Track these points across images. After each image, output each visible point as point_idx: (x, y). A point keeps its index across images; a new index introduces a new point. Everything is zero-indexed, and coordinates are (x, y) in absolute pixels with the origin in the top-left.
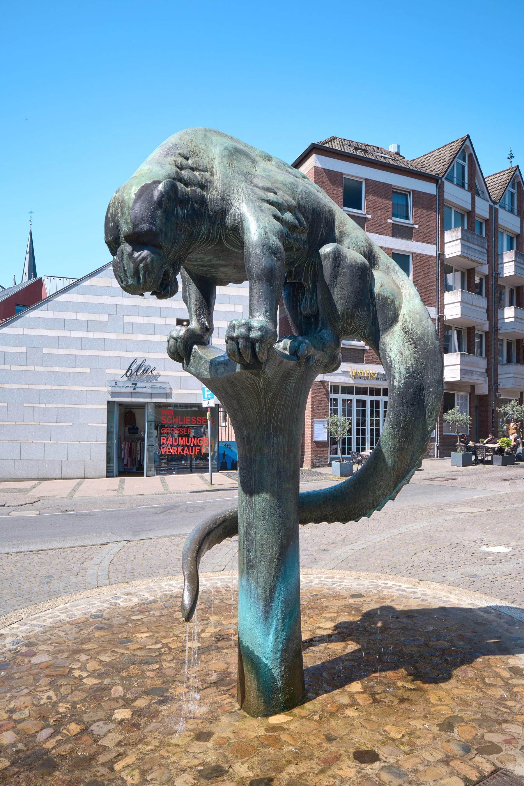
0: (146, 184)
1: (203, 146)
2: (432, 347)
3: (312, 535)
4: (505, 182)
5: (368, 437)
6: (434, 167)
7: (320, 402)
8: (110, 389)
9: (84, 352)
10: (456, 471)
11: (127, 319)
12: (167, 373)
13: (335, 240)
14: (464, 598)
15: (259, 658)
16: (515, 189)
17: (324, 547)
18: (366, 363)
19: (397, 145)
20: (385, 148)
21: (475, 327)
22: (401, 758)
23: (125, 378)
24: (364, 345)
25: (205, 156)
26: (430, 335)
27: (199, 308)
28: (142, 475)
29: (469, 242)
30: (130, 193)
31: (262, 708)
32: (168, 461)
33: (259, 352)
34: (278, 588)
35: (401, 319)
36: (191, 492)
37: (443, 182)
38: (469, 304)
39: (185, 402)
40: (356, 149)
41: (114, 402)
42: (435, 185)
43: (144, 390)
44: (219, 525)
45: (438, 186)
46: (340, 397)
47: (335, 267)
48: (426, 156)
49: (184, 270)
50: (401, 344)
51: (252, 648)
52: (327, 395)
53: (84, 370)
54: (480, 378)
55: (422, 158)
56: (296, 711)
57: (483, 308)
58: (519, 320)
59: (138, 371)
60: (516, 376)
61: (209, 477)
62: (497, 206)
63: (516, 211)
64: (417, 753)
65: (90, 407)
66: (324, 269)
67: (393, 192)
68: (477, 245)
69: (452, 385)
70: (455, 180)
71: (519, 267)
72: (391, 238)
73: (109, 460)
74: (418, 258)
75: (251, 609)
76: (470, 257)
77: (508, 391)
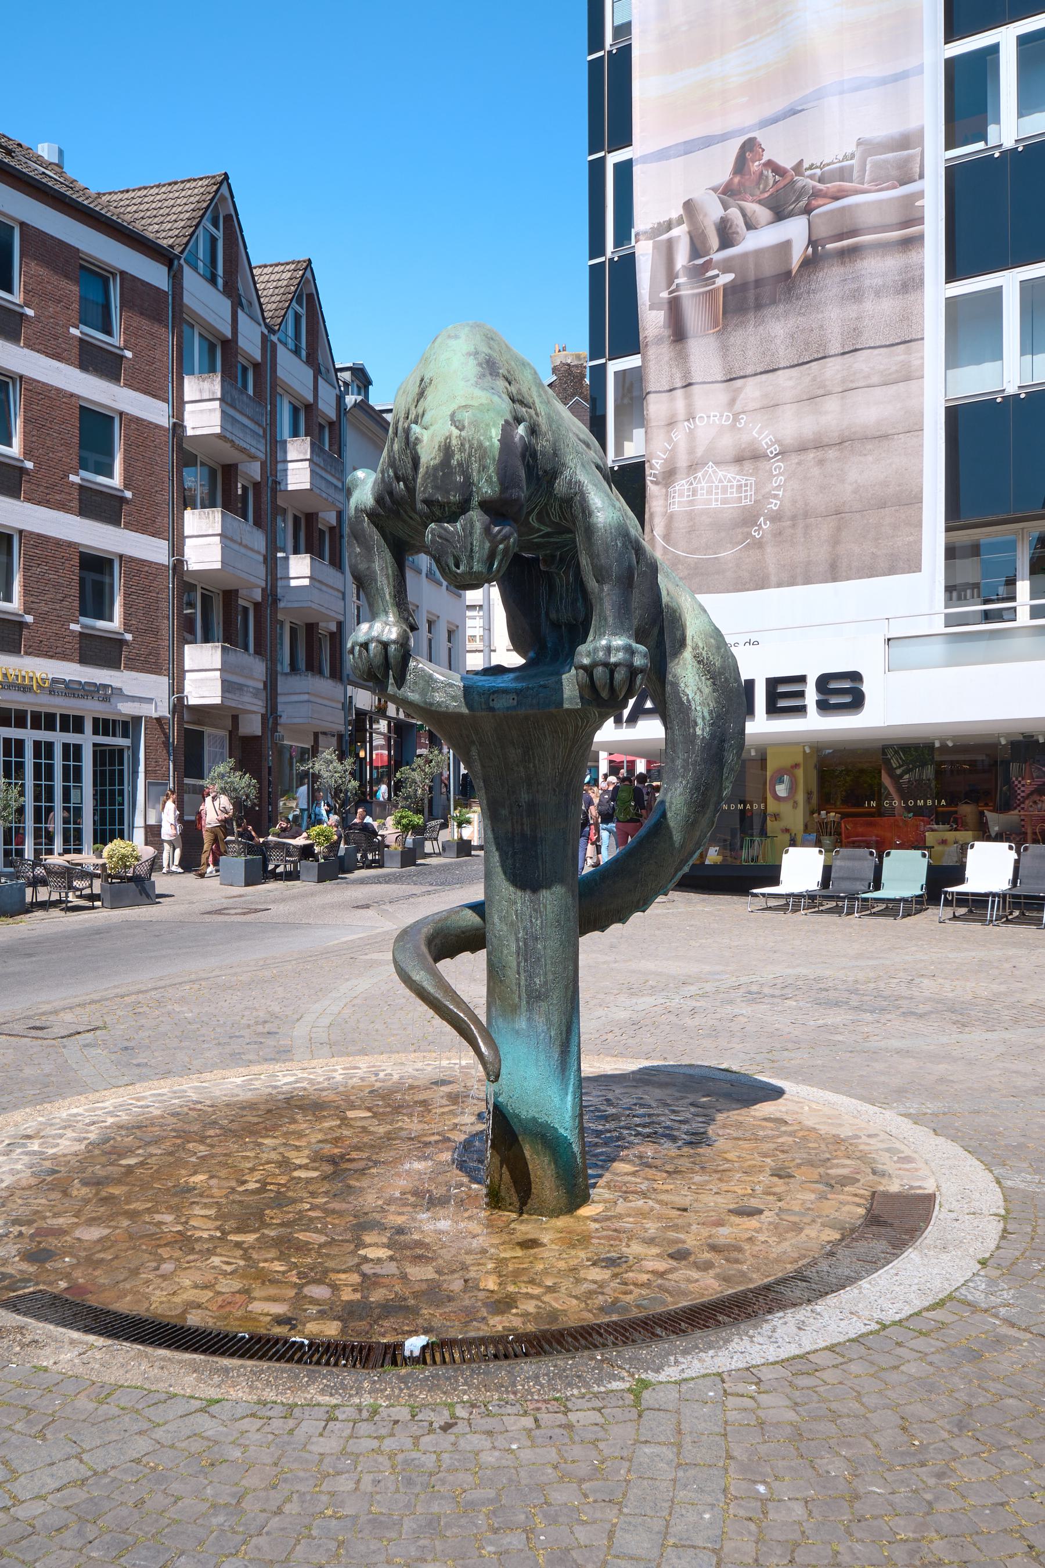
4: (288, 290)
10: (240, 896)
18: (27, 653)
21: (237, 591)
24: (21, 612)
29: (235, 408)
30: (491, 437)
35: (689, 641)
38: (235, 541)
42: (166, 269)
45: (172, 273)
49: (371, 525)
54: (255, 701)
57: (258, 552)
58: (317, 584)
60: (313, 699)
62: (274, 338)
67: (82, 267)
68: (248, 417)
69: (202, 712)
71: (317, 474)
72: (78, 371)
74: (133, 426)
75: (537, 1060)
76: (237, 442)
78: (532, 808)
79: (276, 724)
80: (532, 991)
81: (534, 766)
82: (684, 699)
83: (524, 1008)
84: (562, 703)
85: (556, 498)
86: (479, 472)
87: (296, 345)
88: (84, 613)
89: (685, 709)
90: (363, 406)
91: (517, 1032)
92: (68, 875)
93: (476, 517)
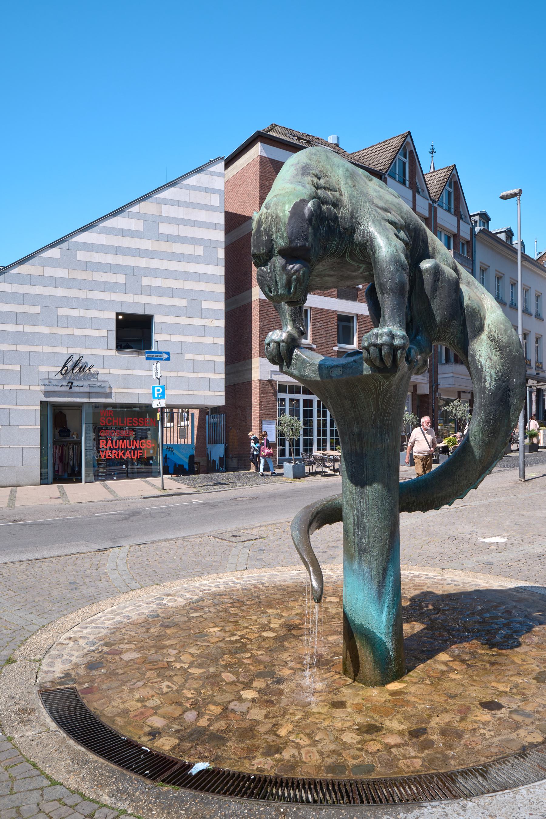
0: (296, 202)
1: (329, 166)
2: (517, 354)
3: (412, 523)
4: (443, 181)
5: (315, 437)
6: (376, 162)
7: (268, 402)
8: (43, 388)
9: (13, 348)
10: (406, 471)
11: (61, 311)
12: (106, 371)
13: (429, 256)
14: (491, 582)
15: (374, 633)
16: (451, 188)
17: (333, 544)
19: (336, 136)
20: (325, 140)
22: (520, 704)
23: (60, 376)
24: (311, 344)
25: (332, 177)
26: (515, 343)
27: (294, 313)
28: (80, 481)
30: (284, 210)
31: (378, 678)
32: (107, 466)
33: (401, 357)
34: (389, 569)
35: (486, 328)
36: (143, 498)
37: (387, 178)
39: (127, 402)
40: (299, 139)
41: (47, 402)
43: (81, 389)
44: (315, 517)
46: (287, 396)
47: (435, 281)
48: (367, 150)
50: (489, 351)
51: (366, 625)
52: (275, 394)
53: (13, 367)
55: (362, 152)
56: (406, 678)
59: (75, 368)
60: (455, 375)
61: (161, 482)
62: (436, 205)
63: (453, 210)
64: (530, 700)
65: (21, 407)
66: (425, 283)
70: (397, 176)
73: (43, 465)
75: (364, 590)
77: (448, 391)
78: (360, 436)
79: (437, 388)
80: (361, 547)
81: (358, 411)
82: (479, 365)
83: (357, 557)
84: (363, 372)
85: (356, 245)
86: (276, 233)
87: (449, 207)
88: (339, 342)
89: (479, 371)
90: (486, 232)
91: (353, 571)
92: (323, 460)
93: (279, 261)
